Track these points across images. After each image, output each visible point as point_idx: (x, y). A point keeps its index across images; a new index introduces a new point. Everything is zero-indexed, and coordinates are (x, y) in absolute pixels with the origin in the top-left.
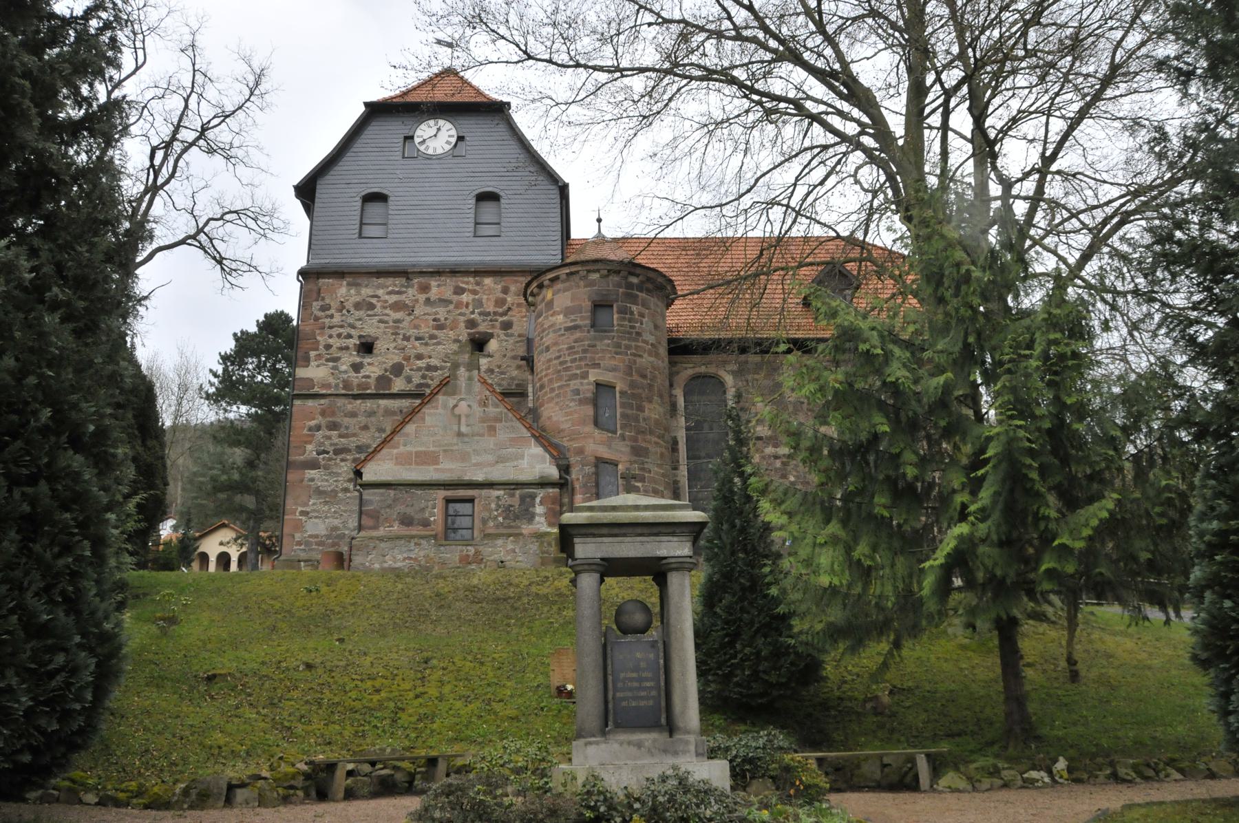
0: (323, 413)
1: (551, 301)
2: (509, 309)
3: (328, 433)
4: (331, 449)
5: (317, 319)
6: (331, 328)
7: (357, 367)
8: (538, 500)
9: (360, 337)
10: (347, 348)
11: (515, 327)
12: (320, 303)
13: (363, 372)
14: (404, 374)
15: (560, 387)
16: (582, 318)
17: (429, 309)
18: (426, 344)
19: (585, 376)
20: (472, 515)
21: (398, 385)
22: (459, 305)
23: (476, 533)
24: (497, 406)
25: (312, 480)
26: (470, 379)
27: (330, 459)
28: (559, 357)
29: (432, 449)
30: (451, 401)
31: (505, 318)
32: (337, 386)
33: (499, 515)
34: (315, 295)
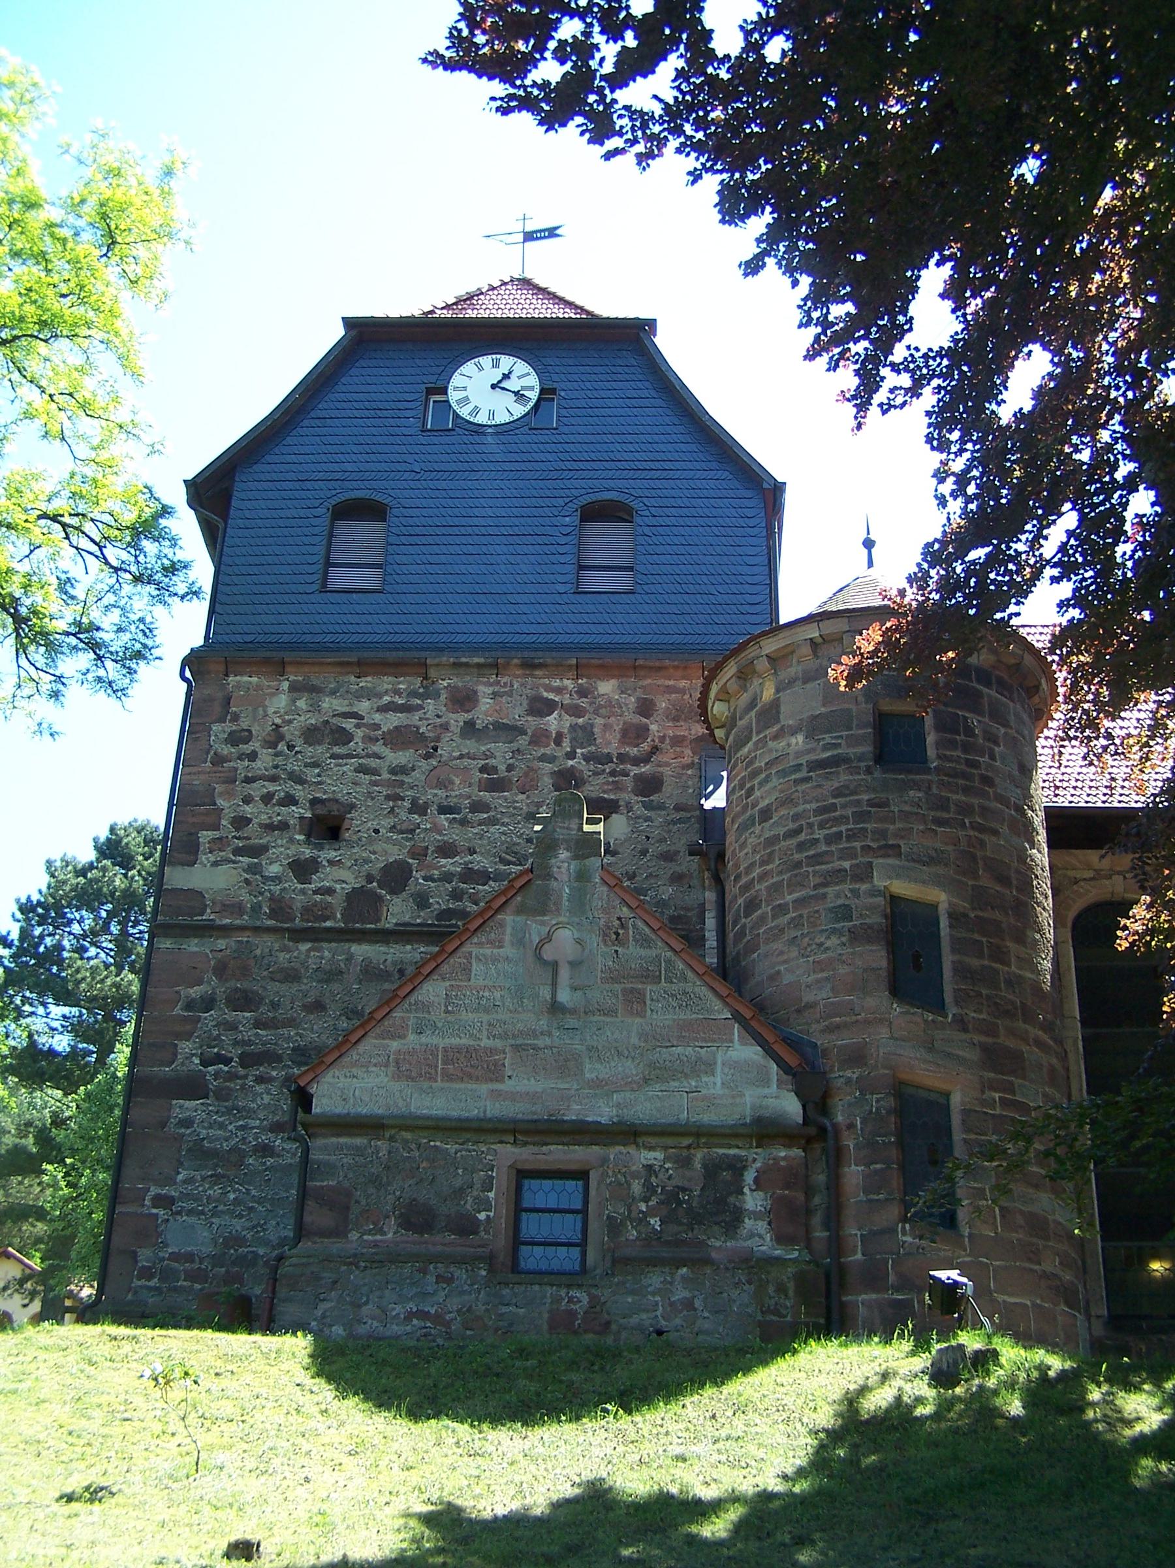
0: (221, 970)
1: (775, 705)
2: (655, 749)
3: (231, 1016)
4: (235, 1053)
5: (219, 760)
6: (248, 780)
7: (303, 869)
8: (749, 1176)
9: (314, 802)
10: (283, 826)
11: (667, 789)
12: (229, 727)
13: (317, 882)
14: (411, 888)
15: (799, 903)
16: (853, 741)
17: (470, 746)
18: (464, 822)
19: (864, 873)
20: (584, 1212)
21: (397, 910)
22: (540, 737)
23: (592, 1256)
24: (646, 942)
25: (187, 1123)
26: (582, 876)
27: (232, 1076)
28: (798, 831)
29: (486, 1042)
30: (535, 930)
31: (645, 769)
32: (256, 908)
33: (651, 1212)
34: (217, 709)
